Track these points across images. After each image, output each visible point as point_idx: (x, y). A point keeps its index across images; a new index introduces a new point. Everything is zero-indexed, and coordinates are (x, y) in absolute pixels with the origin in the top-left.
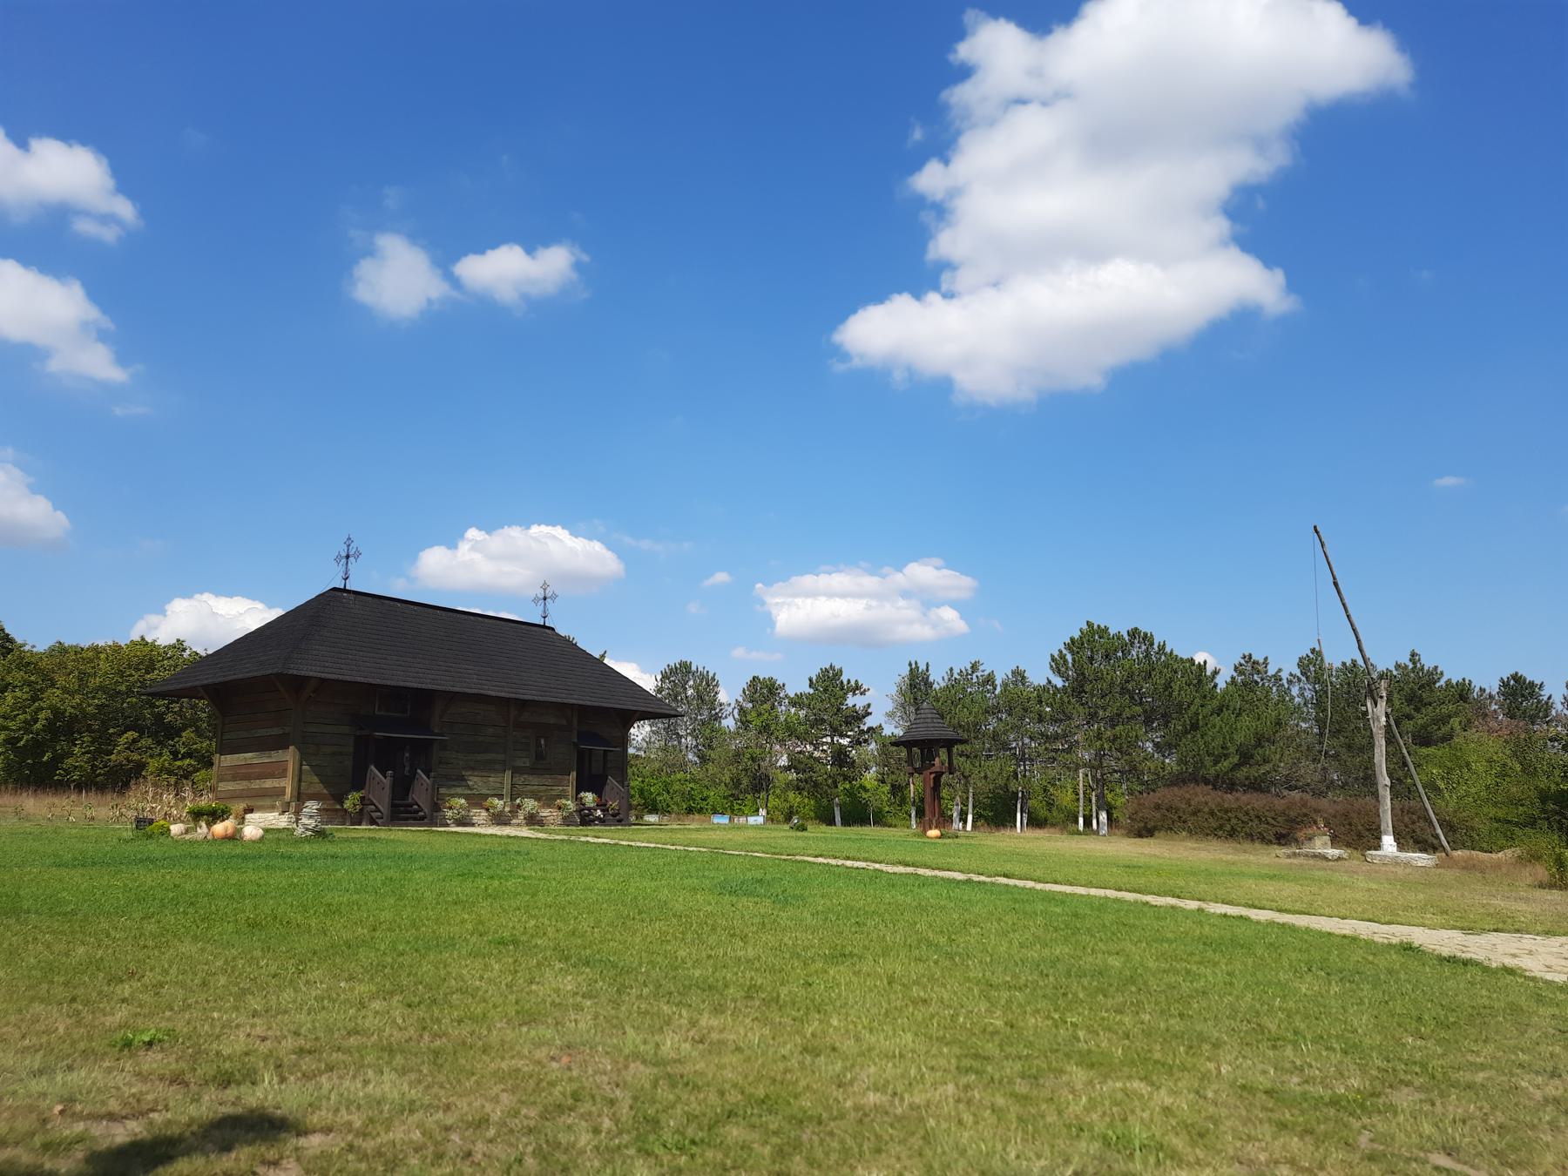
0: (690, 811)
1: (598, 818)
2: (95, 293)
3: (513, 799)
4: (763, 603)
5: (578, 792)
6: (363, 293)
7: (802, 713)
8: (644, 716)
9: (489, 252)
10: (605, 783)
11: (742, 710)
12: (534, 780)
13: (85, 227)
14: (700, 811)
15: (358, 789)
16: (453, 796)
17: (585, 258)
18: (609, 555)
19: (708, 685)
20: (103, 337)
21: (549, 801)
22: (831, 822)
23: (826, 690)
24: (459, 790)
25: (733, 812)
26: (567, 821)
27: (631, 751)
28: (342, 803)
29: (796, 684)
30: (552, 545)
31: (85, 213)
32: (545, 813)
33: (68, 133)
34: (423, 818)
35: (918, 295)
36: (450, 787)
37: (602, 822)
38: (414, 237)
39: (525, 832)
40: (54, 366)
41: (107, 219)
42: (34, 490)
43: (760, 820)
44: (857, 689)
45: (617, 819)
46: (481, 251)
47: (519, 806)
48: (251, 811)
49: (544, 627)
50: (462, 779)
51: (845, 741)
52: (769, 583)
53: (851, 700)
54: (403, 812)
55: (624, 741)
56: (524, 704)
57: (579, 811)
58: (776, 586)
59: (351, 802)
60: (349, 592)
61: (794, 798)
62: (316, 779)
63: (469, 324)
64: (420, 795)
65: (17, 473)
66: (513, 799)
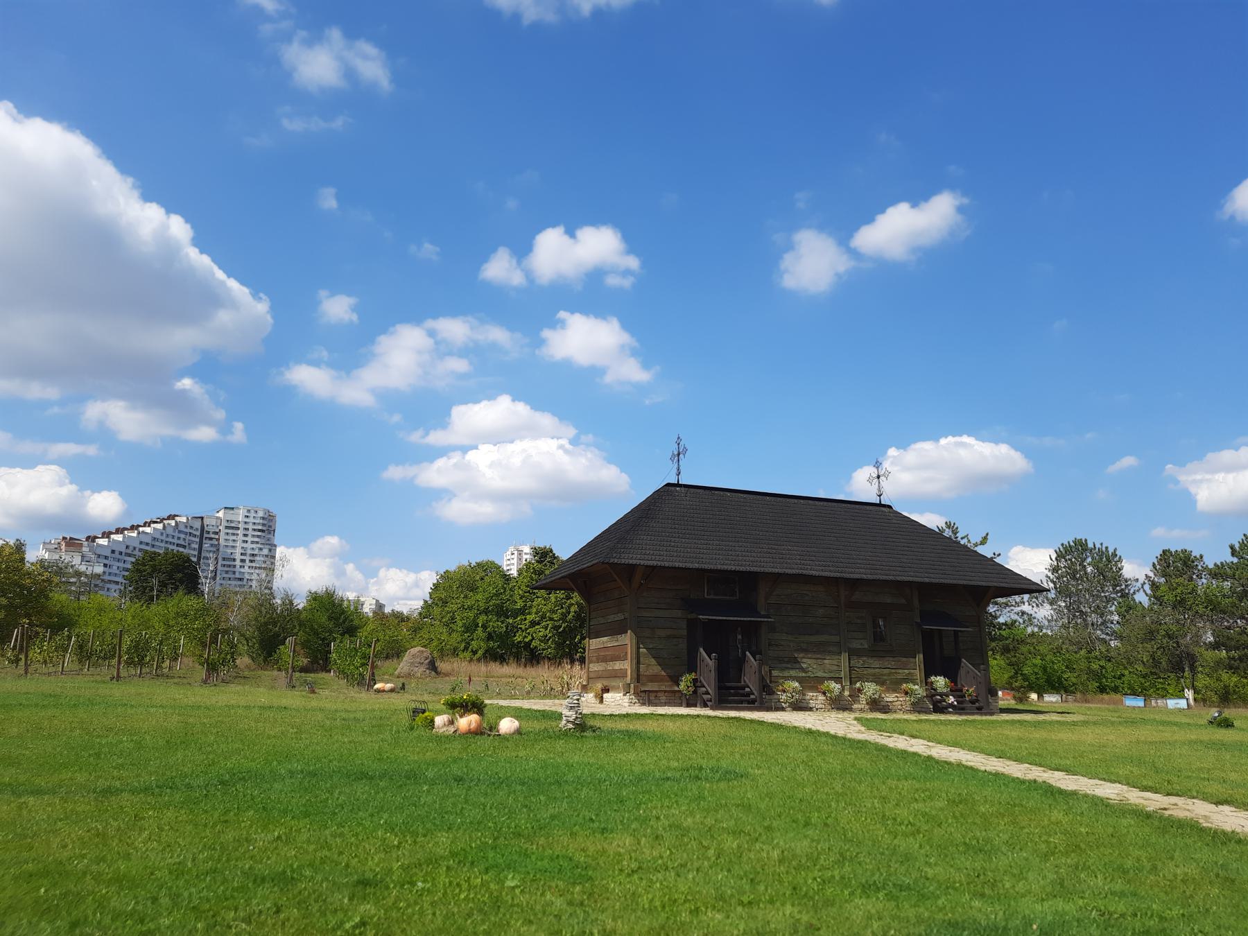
1: (951, 705)
2: (626, 326)
4: (1177, 482)
5: (927, 675)
6: (789, 282)
7: (1227, 584)
11: (1154, 586)
12: (875, 663)
13: (612, 281)
14: (1116, 690)
15: (690, 672)
16: (787, 678)
17: (966, 201)
18: (1013, 453)
19: (1107, 564)
20: (634, 353)
21: (895, 686)
24: (793, 673)
26: (917, 707)
28: (678, 685)
30: (962, 452)
31: (614, 270)
32: (890, 698)
33: (596, 220)
34: (753, 702)
36: (783, 669)
37: (959, 709)
38: (821, 227)
41: (627, 272)
42: (609, 461)
43: (1182, 704)
46: (869, 219)
47: (860, 690)
48: (606, 690)
49: (880, 505)
52: (1181, 463)
54: (730, 693)
56: (854, 584)
57: (931, 697)
58: (1189, 466)
59: (684, 684)
60: (680, 486)
62: (653, 661)
63: (876, 285)
64: (750, 680)
65: (597, 451)
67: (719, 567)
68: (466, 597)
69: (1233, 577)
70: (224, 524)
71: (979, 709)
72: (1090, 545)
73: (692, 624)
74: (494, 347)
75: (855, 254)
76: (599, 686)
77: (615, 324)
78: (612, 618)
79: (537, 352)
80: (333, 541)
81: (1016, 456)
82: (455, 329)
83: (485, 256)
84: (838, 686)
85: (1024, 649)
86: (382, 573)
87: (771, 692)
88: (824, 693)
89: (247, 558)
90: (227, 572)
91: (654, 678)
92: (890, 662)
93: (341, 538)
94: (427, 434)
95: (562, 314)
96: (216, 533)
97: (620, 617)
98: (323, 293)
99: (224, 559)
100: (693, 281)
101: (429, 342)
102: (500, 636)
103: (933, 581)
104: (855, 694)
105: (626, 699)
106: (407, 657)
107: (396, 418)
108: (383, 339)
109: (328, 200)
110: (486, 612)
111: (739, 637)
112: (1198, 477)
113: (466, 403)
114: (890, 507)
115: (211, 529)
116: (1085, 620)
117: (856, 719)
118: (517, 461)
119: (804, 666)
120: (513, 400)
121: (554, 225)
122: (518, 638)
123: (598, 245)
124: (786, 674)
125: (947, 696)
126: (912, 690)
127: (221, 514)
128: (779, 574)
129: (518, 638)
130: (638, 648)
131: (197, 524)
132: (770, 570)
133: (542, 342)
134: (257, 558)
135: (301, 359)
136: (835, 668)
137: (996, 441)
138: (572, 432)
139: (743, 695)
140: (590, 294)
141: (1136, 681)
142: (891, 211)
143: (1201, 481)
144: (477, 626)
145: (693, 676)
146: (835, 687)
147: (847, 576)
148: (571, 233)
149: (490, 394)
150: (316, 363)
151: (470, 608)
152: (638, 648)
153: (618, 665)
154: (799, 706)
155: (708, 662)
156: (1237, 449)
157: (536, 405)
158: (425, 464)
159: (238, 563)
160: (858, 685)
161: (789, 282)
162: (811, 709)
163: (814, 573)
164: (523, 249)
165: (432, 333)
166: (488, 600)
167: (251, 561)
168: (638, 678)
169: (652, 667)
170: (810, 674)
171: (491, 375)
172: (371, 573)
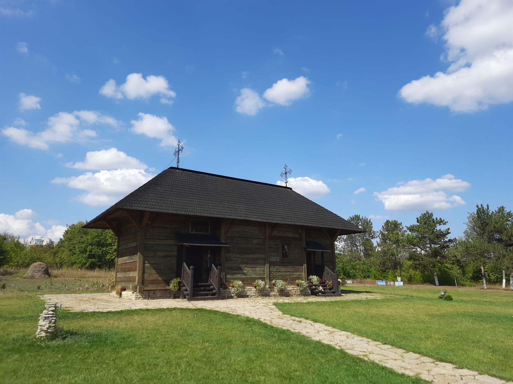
1: (321, 291)
2: (170, 121)
3: (270, 280)
4: (378, 198)
5: (308, 275)
6: (239, 110)
9: (274, 85)
12: (283, 269)
13: (163, 101)
14: (369, 277)
16: (235, 279)
17: (309, 82)
20: (175, 134)
21: (292, 281)
22: (433, 283)
23: (425, 223)
24: (239, 276)
25: (384, 278)
26: (304, 293)
27: (337, 252)
28: (169, 285)
29: (408, 221)
31: (165, 96)
32: (290, 288)
33: (157, 74)
34: (214, 294)
35: (432, 75)
40: (162, 144)
41: (170, 98)
44: (441, 222)
46: (270, 86)
47: (274, 285)
48: (124, 290)
49: (286, 187)
50: (239, 270)
53: (438, 227)
55: (333, 247)
58: (383, 192)
59: (173, 286)
61: (412, 272)
62: (154, 271)
63: (273, 113)
64: (213, 282)
66: (270, 280)
67: (198, 214)
68: (82, 237)
69: (418, 231)
71: (334, 293)
72: (361, 217)
73: (180, 248)
74: (108, 126)
75: (265, 100)
76: (119, 287)
77: (166, 120)
78: (130, 245)
79: (128, 129)
80: (28, 211)
81: (324, 186)
82: (90, 116)
83: (102, 83)
84: (263, 283)
86: (54, 227)
87: (226, 288)
88: (255, 287)
92: (290, 269)
93: (33, 210)
94: (74, 164)
95: (140, 114)
97: (134, 244)
98: (22, 95)
100: (196, 99)
101: (77, 122)
102: (99, 256)
103: (314, 225)
105: (134, 295)
106: (31, 267)
107: (60, 155)
108: (52, 119)
109: (23, 49)
110: (91, 244)
111: (209, 256)
112: (386, 196)
113: (94, 150)
114: (291, 189)
116: (357, 248)
117: (274, 304)
118: (119, 178)
119: (245, 272)
120: (118, 151)
121: (138, 72)
122: (108, 257)
123: (157, 84)
124: (235, 276)
126: (301, 283)
128: (234, 220)
129: (108, 257)
130: (144, 263)
132: (228, 217)
133: (131, 126)
135: (10, 124)
136: (262, 272)
137: (318, 180)
138: (146, 167)
139: (209, 290)
140: (152, 105)
141: (378, 274)
142: (280, 83)
143: (386, 198)
144: (86, 251)
145: (179, 280)
146: (261, 283)
147: (271, 221)
148: (144, 77)
149: (106, 147)
150: (18, 127)
151: (83, 243)
153: (131, 274)
154: (242, 295)
155: (188, 270)
156: (398, 187)
157: (129, 153)
158: (73, 177)
160: (273, 281)
161: (239, 110)
164: (121, 81)
165: (77, 118)
166: (93, 239)
168: (143, 282)
169: (152, 275)
170: (248, 276)
171: (106, 138)
172: (48, 227)
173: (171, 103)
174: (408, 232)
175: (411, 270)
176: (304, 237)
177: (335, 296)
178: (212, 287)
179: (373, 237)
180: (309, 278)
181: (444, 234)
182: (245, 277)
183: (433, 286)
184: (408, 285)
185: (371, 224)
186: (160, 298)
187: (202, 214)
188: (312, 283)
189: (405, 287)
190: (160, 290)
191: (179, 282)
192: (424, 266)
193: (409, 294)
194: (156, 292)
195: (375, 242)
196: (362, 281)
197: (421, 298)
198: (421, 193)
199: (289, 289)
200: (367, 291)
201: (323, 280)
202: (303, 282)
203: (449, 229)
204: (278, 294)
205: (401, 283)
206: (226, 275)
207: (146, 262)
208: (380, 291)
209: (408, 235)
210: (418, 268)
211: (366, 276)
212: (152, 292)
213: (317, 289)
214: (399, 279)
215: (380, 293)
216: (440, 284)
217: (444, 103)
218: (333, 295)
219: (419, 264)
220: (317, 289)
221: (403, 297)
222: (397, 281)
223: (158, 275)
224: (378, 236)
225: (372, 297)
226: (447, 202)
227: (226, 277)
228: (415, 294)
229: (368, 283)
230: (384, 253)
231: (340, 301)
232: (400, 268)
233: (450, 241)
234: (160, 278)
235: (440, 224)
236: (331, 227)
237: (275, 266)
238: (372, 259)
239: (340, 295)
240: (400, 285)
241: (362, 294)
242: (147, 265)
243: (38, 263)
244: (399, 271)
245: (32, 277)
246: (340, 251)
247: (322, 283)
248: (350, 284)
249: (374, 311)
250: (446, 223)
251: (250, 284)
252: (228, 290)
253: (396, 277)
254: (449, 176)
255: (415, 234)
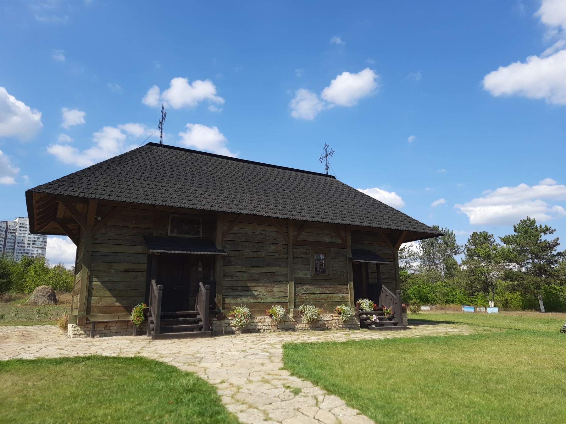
0: (447, 302)
4: (460, 210)
5: (356, 299)
6: (294, 114)
8: (412, 236)
10: (379, 291)
12: (316, 289)
13: (212, 109)
14: (452, 302)
16: (238, 305)
17: (376, 76)
21: (331, 307)
22: (538, 309)
23: (526, 232)
24: (245, 300)
25: (472, 303)
26: (349, 325)
31: (214, 103)
32: (327, 317)
33: (203, 79)
36: (235, 297)
39: (315, 337)
41: (219, 106)
44: (546, 230)
45: (395, 322)
46: (328, 84)
47: (302, 312)
49: (327, 176)
51: (542, 262)
53: (544, 238)
56: (302, 225)
59: (134, 317)
61: (508, 295)
62: (108, 293)
63: (335, 116)
69: (516, 242)
70: (19, 225)
71: (395, 324)
73: (151, 257)
75: (327, 103)
83: (144, 93)
85: (410, 281)
88: (271, 316)
89: (31, 243)
90: (20, 250)
91: (106, 310)
92: (328, 289)
95: (188, 125)
96: (14, 230)
98: (64, 110)
99: (18, 243)
101: (123, 137)
103: (363, 224)
104: (298, 315)
111: (200, 269)
112: (470, 209)
114: (334, 177)
115: (11, 228)
121: (184, 77)
123: (204, 89)
124: (239, 301)
125: (371, 315)
126: (344, 311)
127: (17, 220)
130: (91, 281)
131: (4, 225)
134: (36, 243)
136: (283, 294)
137: (390, 192)
143: (471, 210)
146: (280, 310)
148: (190, 83)
150: (63, 144)
152: (91, 281)
154: (248, 329)
159: (26, 245)
160: (301, 308)
161: (294, 114)
162: (258, 331)
163: (265, 214)
164: (165, 86)
165: (123, 132)
167: (33, 244)
168: (88, 309)
169: (104, 298)
170: (260, 300)
173: (220, 111)
174: (502, 244)
175: (507, 293)
176: (349, 242)
177: (397, 329)
178: (198, 317)
179: (456, 253)
180: (358, 302)
181: (550, 246)
182: (255, 301)
183: (538, 313)
184: (505, 312)
185: (454, 237)
186: (116, 334)
187: (179, 205)
188: (362, 310)
189: (501, 314)
190: (117, 322)
191: (144, 310)
192: (525, 288)
193: (512, 325)
194: (109, 325)
195: (459, 258)
196: (443, 307)
197: (535, 333)
198: (514, 204)
199: (325, 319)
200: (448, 320)
201: (380, 306)
202: (348, 308)
203: (558, 239)
204: (308, 326)
205: (496, 310)
206: (223, 299)
207: (95, 279)
208: (467, 321)
209: (503, 247)
210: (517, 290)
211: (449, 300)
212: (103, 325)
213: (369, 319)
214: (491, 304)
215: (468, 324)
216: (548, 310)
217: (539, 95)
218: (394, 328)
219: (518, 285)
220: (369, 319)
221: (504, 331)
222: (489, 307)
223: (114, 299)
224: (463, 251)
225: (455, 330)
226: (547, 213)
227: (224, 301)
228: (519, 325)
229: (450, 309)
230: (472, 272)
231: (401, 339)
232: (493, 290)
233: (559, 254)
234: (118, 304)
235: (545, 234)
236: (389, 227)
237: (303, 284)
238: (456, 279)
239: (405, 328)
240: (493, 312)
241: (440, 325)
242: (96, 283)
243: (42, 287)
244: (491, 294)
245: (35, 303)
246: (415, 271)
247: (378, 310)
248: (427, 310)
249: (457, 358)
250: (553, 231)
251: (263, 312)
252: (226, 321)
253: (487, 302)
254: (548, 180)
255: (512, 246)
